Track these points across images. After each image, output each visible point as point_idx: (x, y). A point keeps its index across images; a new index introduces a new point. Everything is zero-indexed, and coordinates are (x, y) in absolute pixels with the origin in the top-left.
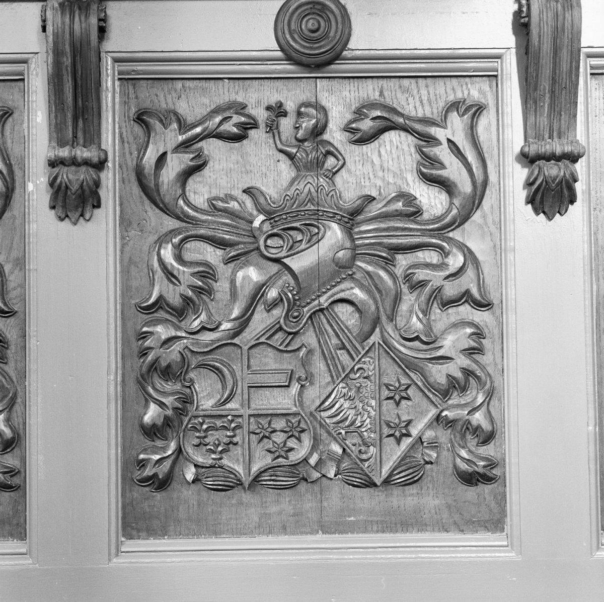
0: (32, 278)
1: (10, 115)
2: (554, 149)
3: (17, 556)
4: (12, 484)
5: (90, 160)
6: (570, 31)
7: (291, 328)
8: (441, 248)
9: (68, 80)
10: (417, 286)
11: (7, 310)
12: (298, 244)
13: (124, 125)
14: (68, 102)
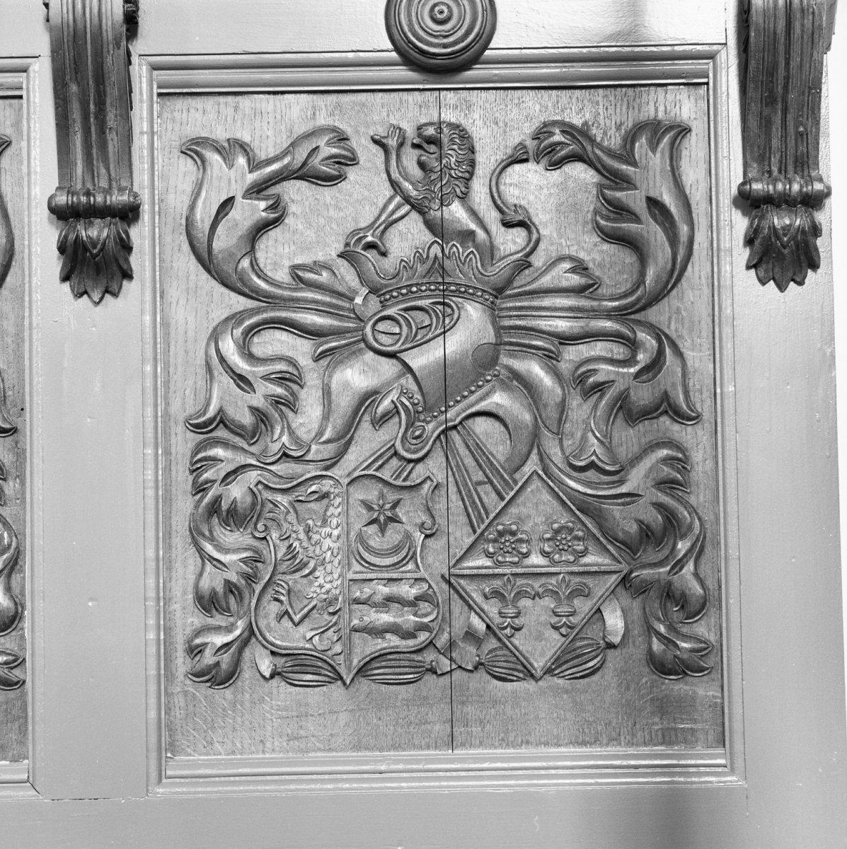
4: (4, 680)
12: (423, 332)
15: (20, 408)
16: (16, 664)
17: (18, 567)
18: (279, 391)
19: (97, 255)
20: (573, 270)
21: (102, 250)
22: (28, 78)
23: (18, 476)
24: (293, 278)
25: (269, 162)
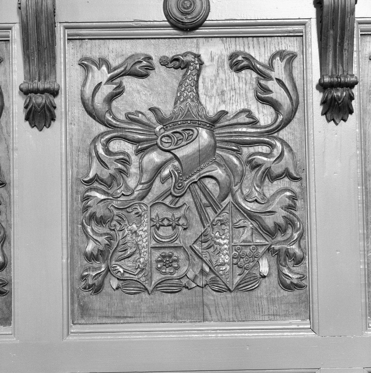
2: (39, 86)
6: (46, 13)
7: (178, 193)
15: (303, 169)
16: (304, 278)
17: (303, 237)
18: (120, 166)
19: (340, 104)
20: (247, 116)
21: (342, 101)
22: (305, 28)
23: (302, 198)
24: (126, 118)
25: (115, 69)
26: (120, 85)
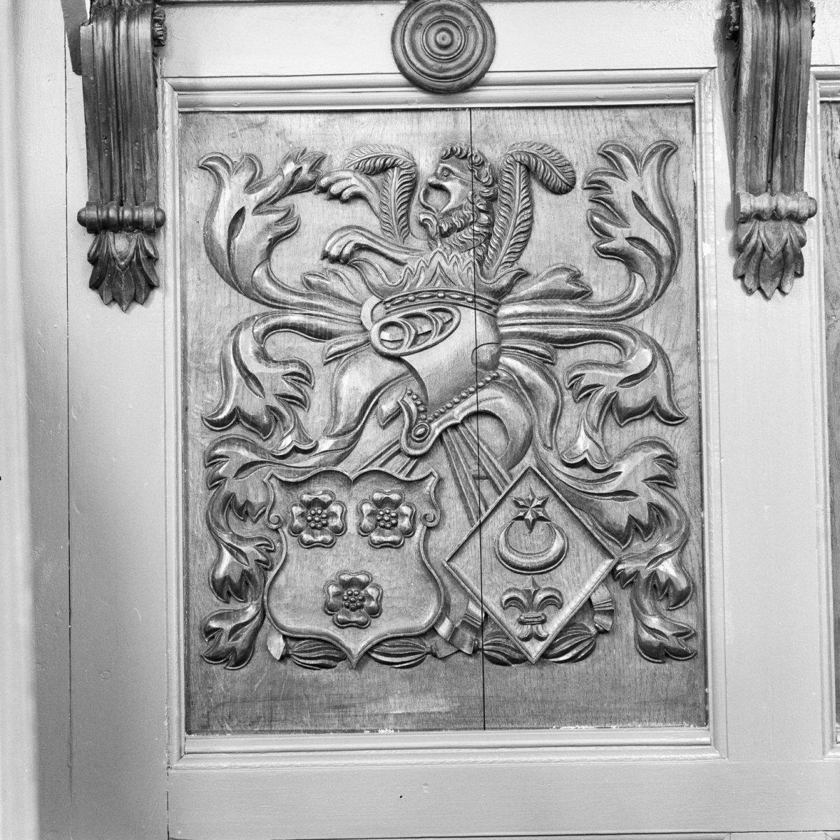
0: (710, 372)
1: (675, 151)
3: (697, 747)
5: (798, 213)
8: (619, 342)
9: (767, 104)
10: (583, 394)
11: (676, 415)
13: (827, 164)
14: (764, 133)
26: (289, 212)
